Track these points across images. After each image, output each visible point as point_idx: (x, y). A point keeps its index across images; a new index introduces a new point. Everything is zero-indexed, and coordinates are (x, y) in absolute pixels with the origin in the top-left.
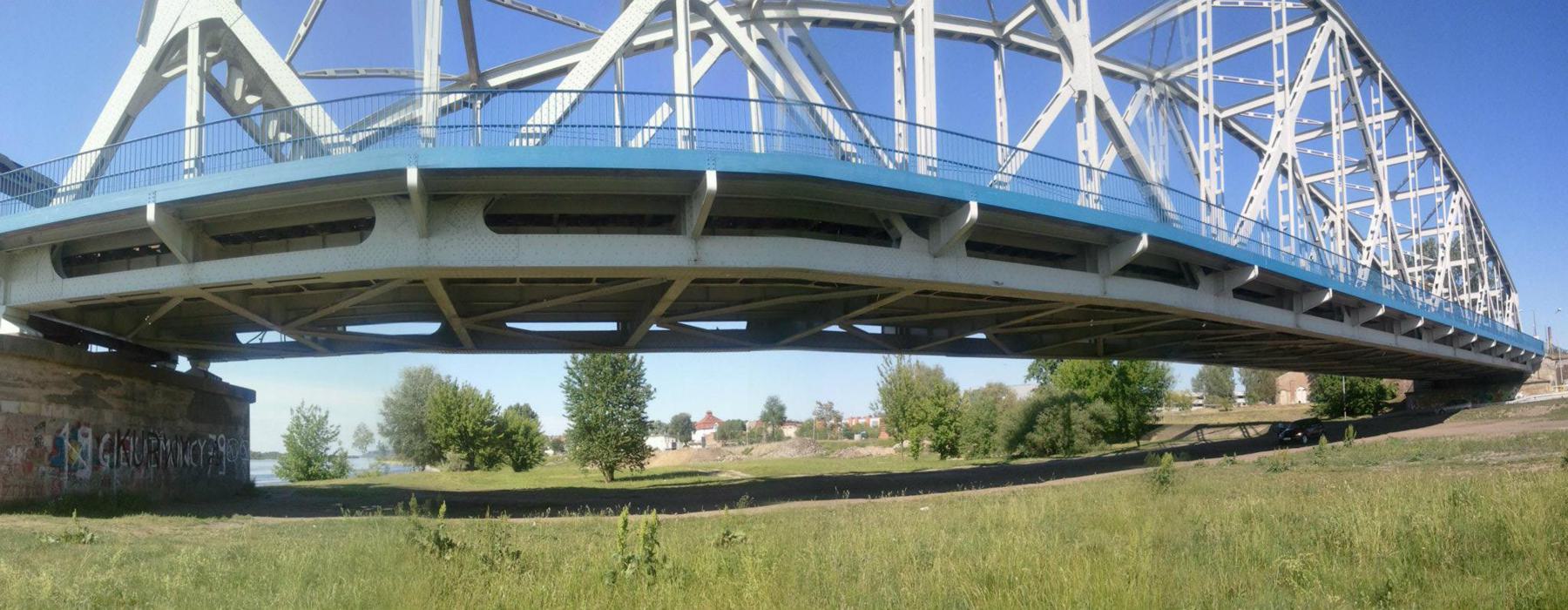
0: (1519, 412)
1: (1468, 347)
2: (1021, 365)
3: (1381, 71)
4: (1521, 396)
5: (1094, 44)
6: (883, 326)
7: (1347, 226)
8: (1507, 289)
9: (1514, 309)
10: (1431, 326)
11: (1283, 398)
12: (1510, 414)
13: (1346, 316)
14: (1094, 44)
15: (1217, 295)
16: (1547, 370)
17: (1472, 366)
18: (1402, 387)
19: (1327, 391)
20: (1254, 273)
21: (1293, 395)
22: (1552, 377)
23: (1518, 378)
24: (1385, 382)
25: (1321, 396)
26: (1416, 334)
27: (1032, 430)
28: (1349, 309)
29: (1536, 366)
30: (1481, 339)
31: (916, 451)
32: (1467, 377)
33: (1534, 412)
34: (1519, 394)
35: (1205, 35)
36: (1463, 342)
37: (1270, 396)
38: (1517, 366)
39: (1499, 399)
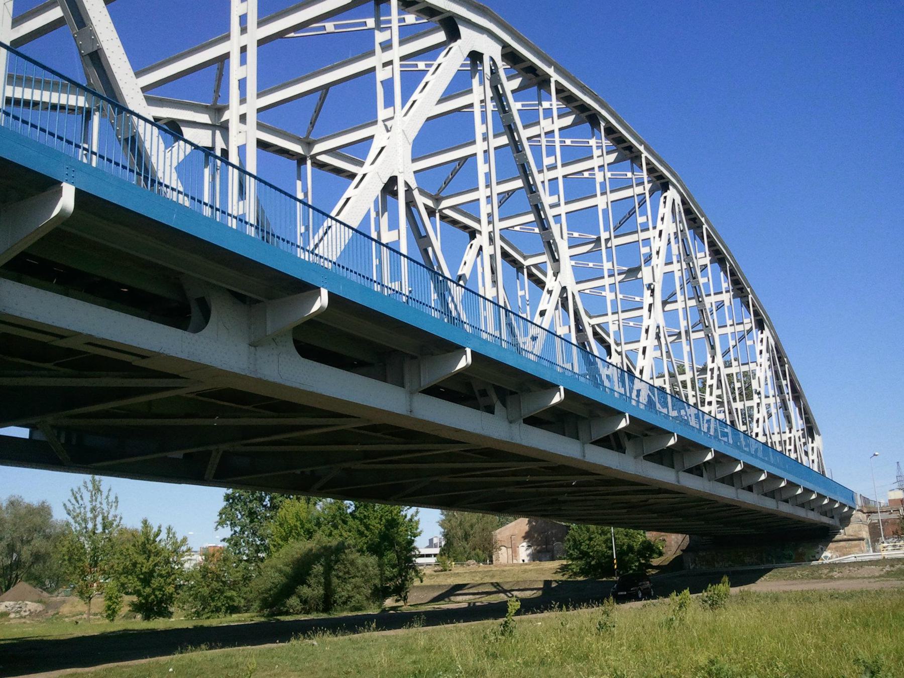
0: (846, 572)
1: (697, 470)
2: (212, 498)
3: (645, 154)
4: (829, 555)
5: (414, 160)
6: (33, 428)
7: (499, 243)
8: (810, 430)
9: (819, 455)
10: (643, 431)
11: (503, 556)
12: (836, 574)
13: (498, 407)
14: (414, 160)
15: (635, 458)
16: (858, 526)
17: (771, 516)
18: (672, 544)
19: (584, 547)
20: (465, 362)
21: (515, 553)
22: (865, 533)
23: (823, 535)
24: (651, 536)
25: (575, 553)
26: (615, 442)
27: (303, 582)
28: (504, 395)
29: (845, 520)
30: (720, 457)
31: (111, 613)
32: (755, 529)
33: (866, 571)
34: (827, 553)
35: (484, 120)
36: (722, 472)
37: (486, 551)
38: (825, 520)
39: (800, 559)
